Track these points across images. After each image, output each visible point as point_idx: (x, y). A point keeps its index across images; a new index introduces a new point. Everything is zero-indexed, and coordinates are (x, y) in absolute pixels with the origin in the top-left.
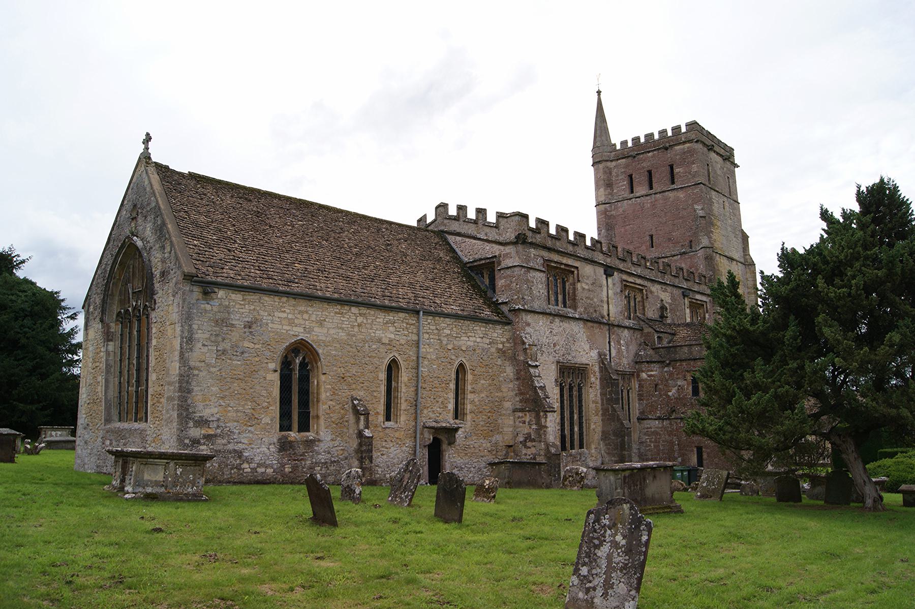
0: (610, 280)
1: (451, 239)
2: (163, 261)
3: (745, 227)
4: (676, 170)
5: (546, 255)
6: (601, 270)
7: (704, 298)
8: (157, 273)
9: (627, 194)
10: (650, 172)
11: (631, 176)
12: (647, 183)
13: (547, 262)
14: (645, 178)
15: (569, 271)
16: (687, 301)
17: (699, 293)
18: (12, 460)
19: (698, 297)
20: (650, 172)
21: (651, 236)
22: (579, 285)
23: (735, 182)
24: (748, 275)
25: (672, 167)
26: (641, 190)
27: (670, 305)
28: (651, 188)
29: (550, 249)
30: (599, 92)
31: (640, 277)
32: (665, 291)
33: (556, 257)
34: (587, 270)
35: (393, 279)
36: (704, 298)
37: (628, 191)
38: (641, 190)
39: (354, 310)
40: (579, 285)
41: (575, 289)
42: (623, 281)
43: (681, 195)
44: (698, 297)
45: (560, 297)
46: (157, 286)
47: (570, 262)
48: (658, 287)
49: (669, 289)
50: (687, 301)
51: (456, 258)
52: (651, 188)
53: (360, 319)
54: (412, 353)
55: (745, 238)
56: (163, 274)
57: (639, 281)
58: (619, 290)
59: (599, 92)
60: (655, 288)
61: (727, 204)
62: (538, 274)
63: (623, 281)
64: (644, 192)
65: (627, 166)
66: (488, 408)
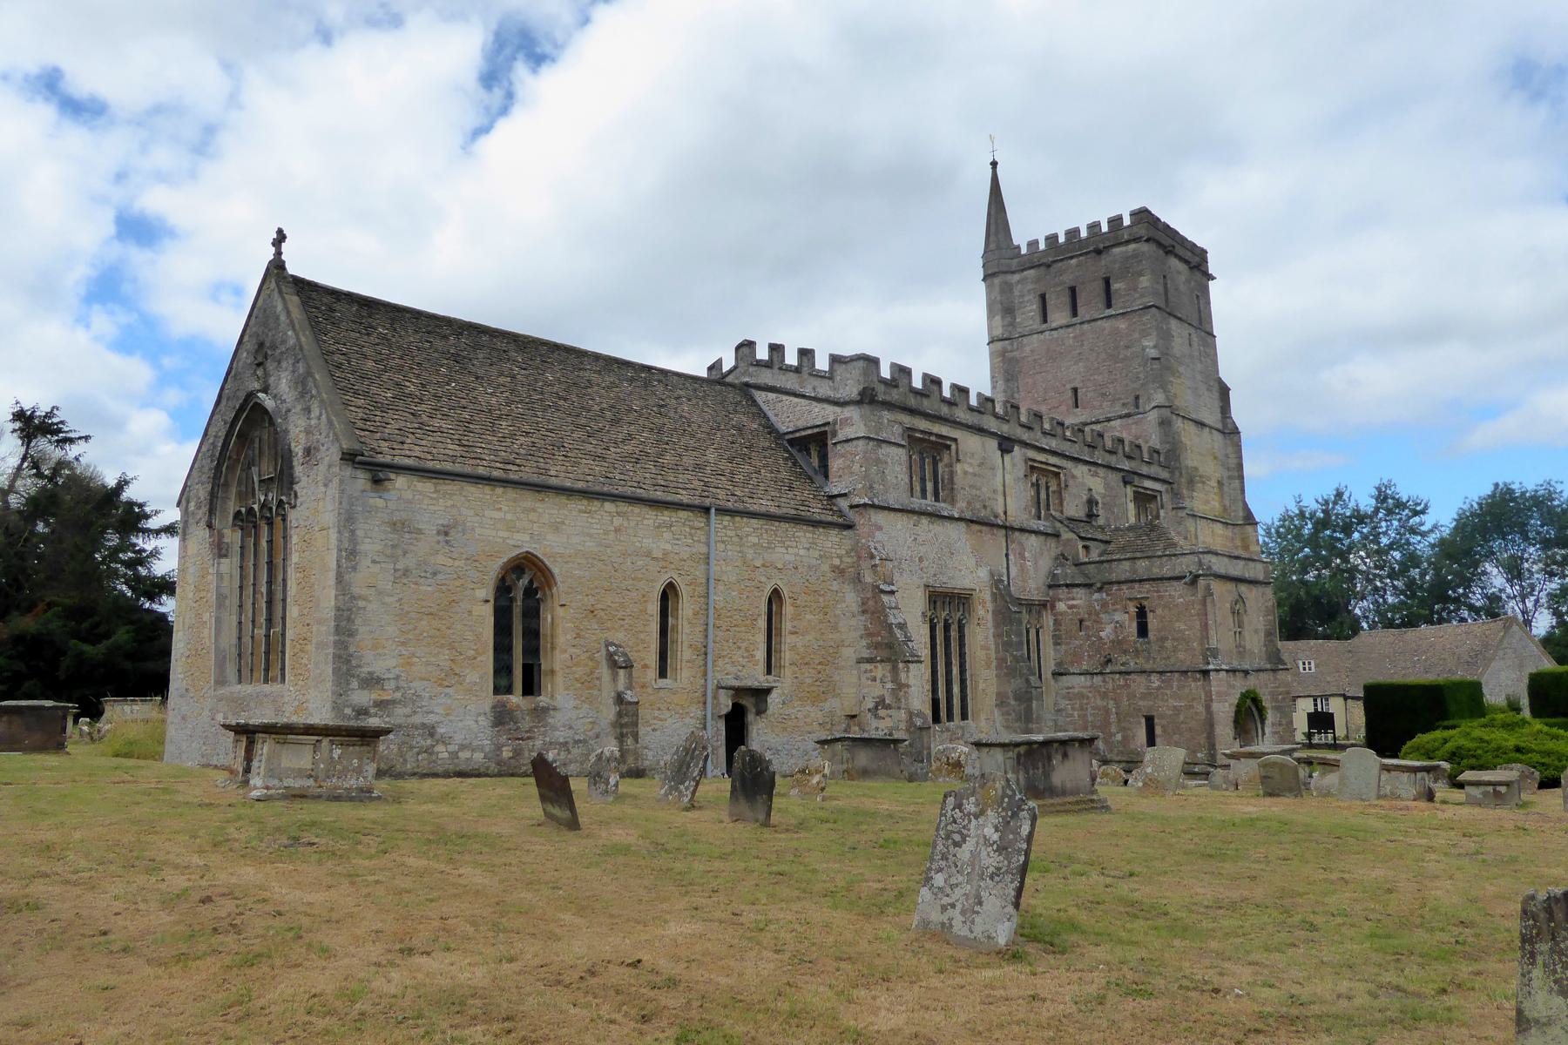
0: (1007, 458)
1: (760, 396)
3: (1224, 374)
4: (1115, 286)
5: (907, 420)
6: (993, 444)
8: (298, 450)
9: (1036, 324)
11: (1043, 297)
13: (909, 432)
14: (1066, 299)
16: (1129, 490)
19: (1148, 484)
21: (1075, 390)
23: (1209, 303)
24: (1230, 449)
26: (1059, 317)
29: (912, 412)
32: (1096, 475)
33: (923, 424)
34: (970, 443)
35: (668, 459)
36: (1157, 486)
37: (1038, 319)
38: (1059, 317)
39: (608, 506)
40: (958, 468)
41: (952, 474)
43: (1122, 325)
44: (1148, 484)
45: (929, 486)
46: (298, 470)
47: (945, 430)
50: (1129, 490)
51: (771, 429)
52: (1075, 313)
53: (617, 521)
54: (699, 572)
55: (1224, 391)
56: (308, 451)
58: (1021, 474)
60: (1080, 471)
61: (1195, 339)
64: (1064, 322)
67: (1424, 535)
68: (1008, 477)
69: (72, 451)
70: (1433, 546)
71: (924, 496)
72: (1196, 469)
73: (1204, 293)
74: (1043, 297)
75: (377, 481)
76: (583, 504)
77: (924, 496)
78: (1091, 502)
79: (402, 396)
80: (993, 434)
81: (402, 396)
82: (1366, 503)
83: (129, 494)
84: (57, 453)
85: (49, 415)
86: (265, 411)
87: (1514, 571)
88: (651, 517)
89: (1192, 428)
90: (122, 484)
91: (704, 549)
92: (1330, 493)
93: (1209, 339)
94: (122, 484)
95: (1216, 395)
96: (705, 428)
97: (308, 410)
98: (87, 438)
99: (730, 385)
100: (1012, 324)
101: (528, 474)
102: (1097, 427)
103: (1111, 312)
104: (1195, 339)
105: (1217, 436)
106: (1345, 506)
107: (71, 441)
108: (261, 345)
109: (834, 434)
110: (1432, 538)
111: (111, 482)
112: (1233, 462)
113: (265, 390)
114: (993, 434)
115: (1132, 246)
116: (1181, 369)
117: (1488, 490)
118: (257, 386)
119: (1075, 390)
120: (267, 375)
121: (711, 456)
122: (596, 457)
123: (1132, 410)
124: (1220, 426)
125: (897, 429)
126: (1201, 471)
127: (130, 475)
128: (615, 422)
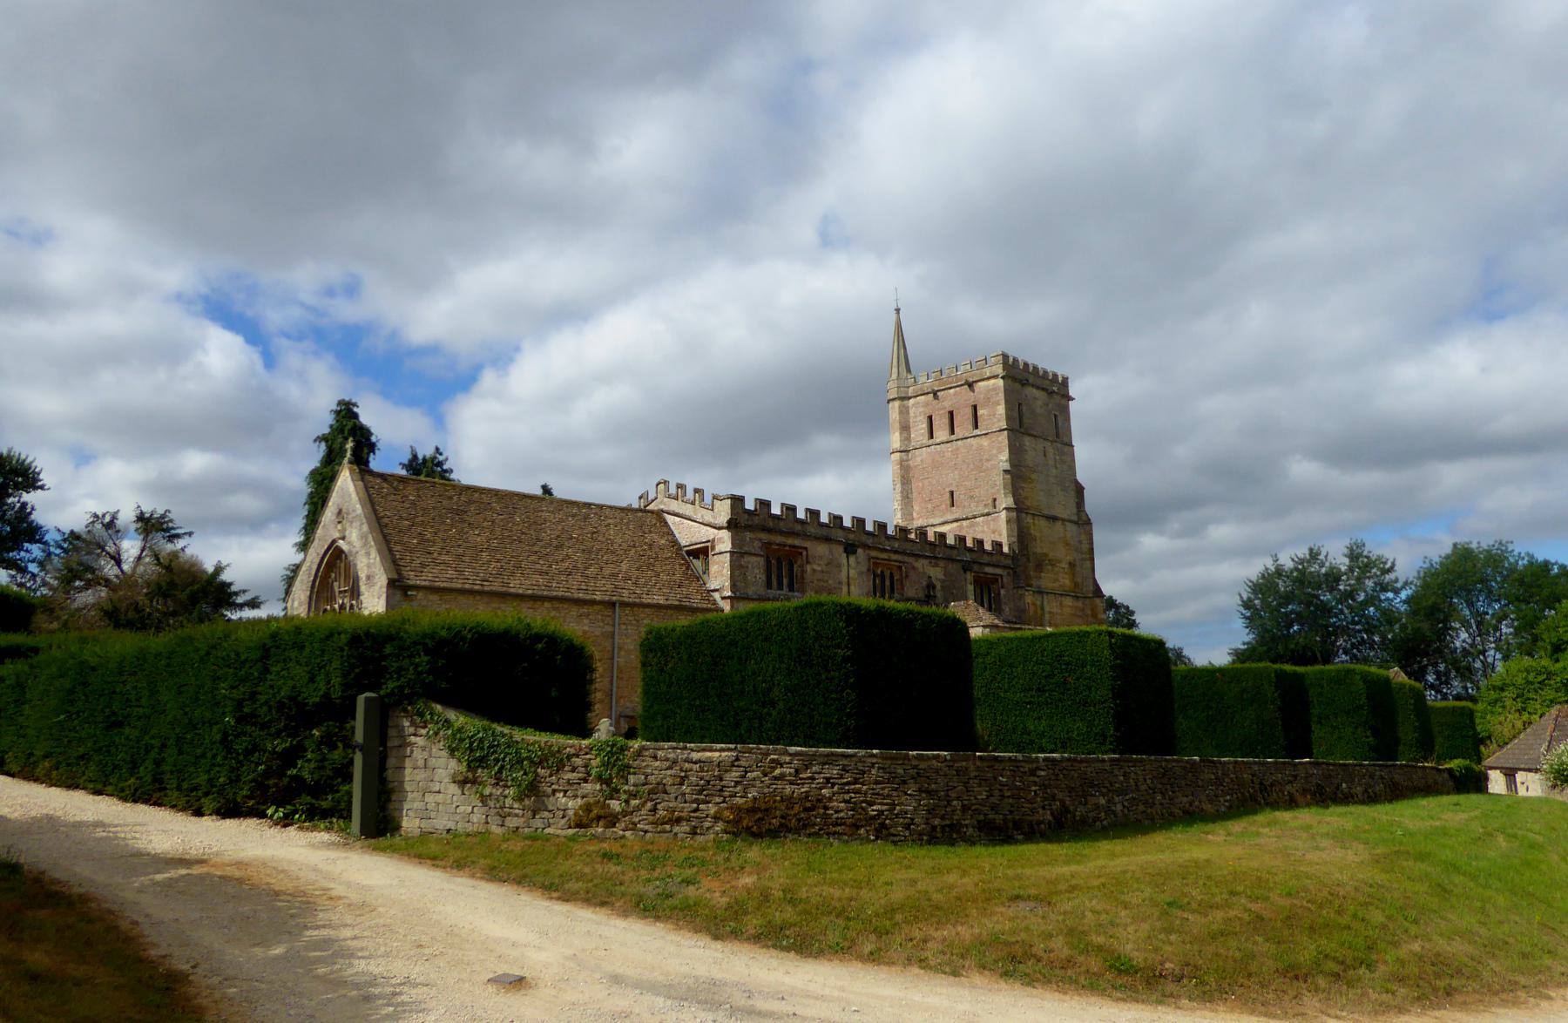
0: (852, 559)
1: (670, 519)
2: (369, 566)
3: (1080, 477)
4: (980, 412)
5: (765, 536)
6: (841, 549)
7: (998, 571)
8: (362, 576)
9: (926, 441)
10: (951, 413)
11: (930, 418)
12: (947, 427)
13: (767, 545)
14: (946, 421)
15: (796, 552)
16: (969, 576)
17: (988, 565)
18: (1474, 783)
19: (989, 570)
20: (951, 413)
21: (952, 493)
22: (809, 568)
23: (1068, 419)
24: (1083, 537)
25: (975, 407)
26: (941, 434)
27: (943, 581)
28: (952, 432)
29: (769, 531)
30: (898, 310)
31: (896, 552)
32: (936, 565)
33: (779, 539)
34: (821, 549)
35: (592, 570)
36: (998, 571)
37: (947, 432)
38: (941, 434)
39: (547, 604)
40: (809, 568)
41: (803, 572)
42: (870, 558)
43: (985, 442)
44: (989, 570)
45: (785, 581)
46: (363, 588)
47: (797, 542)
48: (926, 562)
49: (942, 563)
50: (969, 576)
51: (675, 543)
52: (952, 432)
53: (553, 613)
54: (608, 644)
55: (1080, 490)
56: (368, 577)
57: (894, 557)
58: (864, 569)
59: (898, 310)
60: (920, 564)
61: (1050, 450)
62: (755, 559)
63: (870, 558)
64: (944, 438)
65: (927, 404)
66: (1520, 680)
67: (1397, 592)
68: (852, 572)
69: (180, 544)
70: (1404, 602)
71: (780, 587)
72: (1045, 555)
73: (1065, 411)
74: (930, 418)
75: (406, 595)
76: (530, 604)
77: (780, 587)
78: (931, 586)
79: (422, 540)
80: (840, 542)
81: (422, 540)
82: (1343, 563)
83: (225, 577)
84: (170, 547)
85: (163, 516)
86: (342, 551)
87: (1482, 627)
88: (575, 611)
89: (1043, 522)
90: (219, 569)
91: (609, 629)
92: (1303, 552)
93: (1066, 449)
94: (219, 569)
95: (1073, 493)
96: (625, 546)
97: (368, 554)
98: (190, 534)
99: (652, 512)
100: (908, 439)
101: (496, 587)
102: (939, 529)
103: (977, 432)
104: (1050, 450)
105: (1071, 528)
106: (1322, 565)
107: (178, 536)
108: (340, 512)
109: (713, 548)
110: (1403, 595)
111: (210, 569)
112: (1085, 547)
113: (343, 538)
114: (840, 542)
115: (992, 381)
116: (1033, 476)
117: (1448, 550)
118: (337, 535)
119: (952, 493)
120: (344, 530)
121: (624, 567)
122: (541, 573)
123: (991, 510)
124: (1074, 518)
125: (757, 544)
126: (1051, 555)
127: (224, 563)
128: (559, 547)
